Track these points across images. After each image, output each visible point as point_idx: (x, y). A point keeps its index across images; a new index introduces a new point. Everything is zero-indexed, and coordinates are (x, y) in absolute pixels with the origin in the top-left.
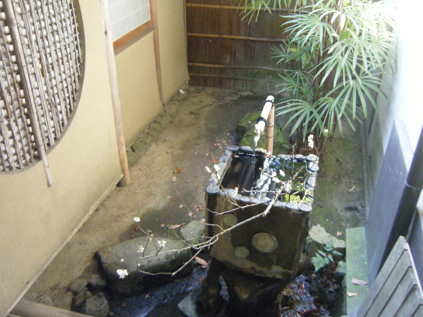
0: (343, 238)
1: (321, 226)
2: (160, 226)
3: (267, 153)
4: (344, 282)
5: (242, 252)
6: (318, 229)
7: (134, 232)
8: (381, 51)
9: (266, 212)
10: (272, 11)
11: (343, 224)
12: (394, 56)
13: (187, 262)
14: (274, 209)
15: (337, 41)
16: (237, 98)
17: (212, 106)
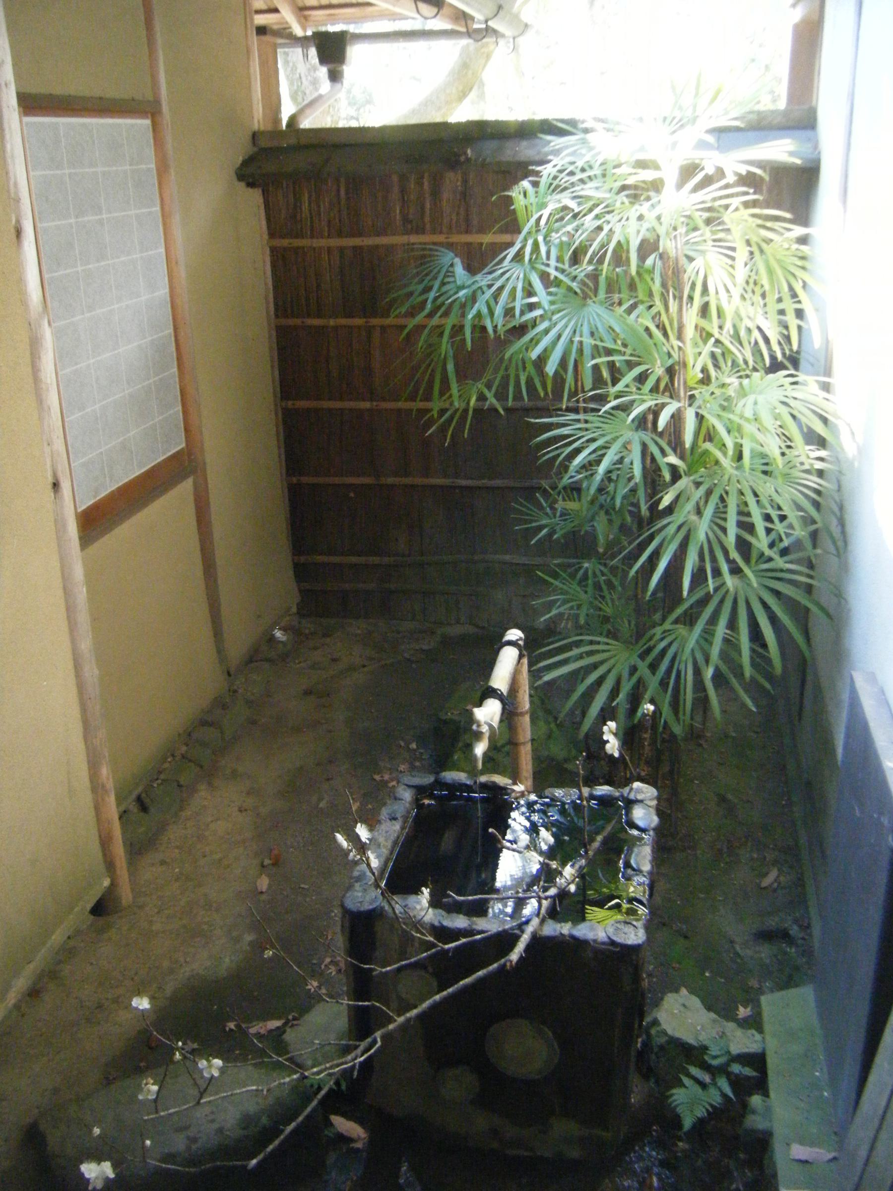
0: (755, 1023)
1: (692, 992)
2: (225, 1026)
3: (516, 788)
4: (771, 1158)
5: (459, 1084)
6: (681, 1001)
7: (145, 1052)
8: (800, 495)
9: (514, 956)
10: (507, 410)
11: (754, 983)
12: (836, 509)
13: (293, 1125)
14: (537, 941)
15: (680, 477)
16: (432, 644)
17: (365, 669)
